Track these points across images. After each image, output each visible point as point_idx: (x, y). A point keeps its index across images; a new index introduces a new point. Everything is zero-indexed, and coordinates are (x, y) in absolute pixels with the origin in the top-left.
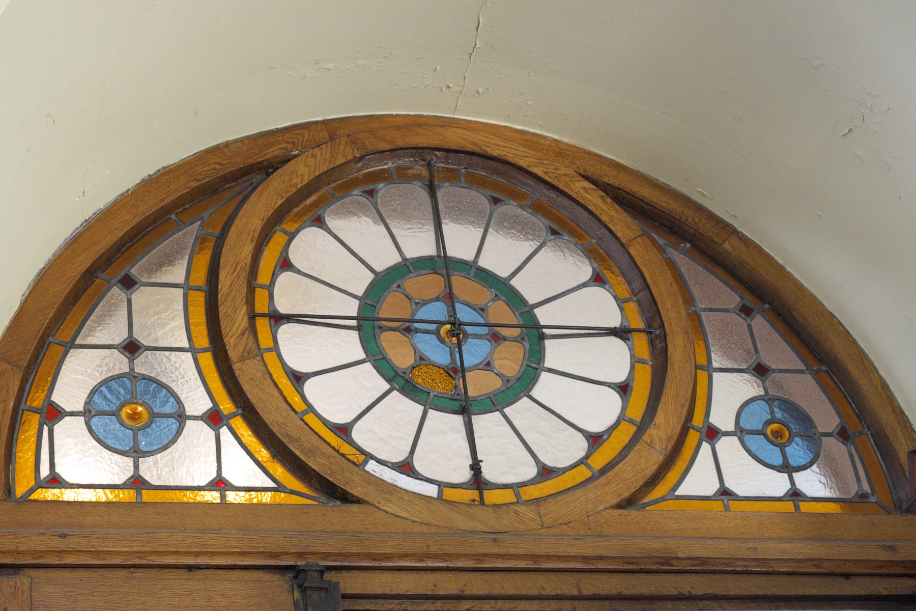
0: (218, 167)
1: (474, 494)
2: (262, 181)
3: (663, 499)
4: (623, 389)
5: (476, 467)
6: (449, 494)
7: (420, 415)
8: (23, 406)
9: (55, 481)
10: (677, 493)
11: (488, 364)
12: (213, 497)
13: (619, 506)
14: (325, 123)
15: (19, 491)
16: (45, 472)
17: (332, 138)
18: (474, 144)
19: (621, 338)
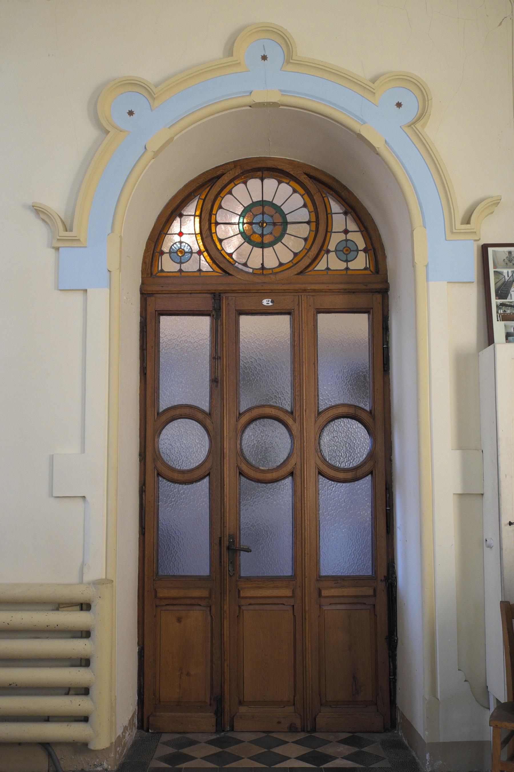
0: (204, 179)
1: (261, 271)
2: (217, 181)
3: (310, 271)
4: (306, 239)
5: (262, 264)
6: (255, 272)
7: (251, 248)
8: (155, 251)
9: (162, 271)
10: (315, 269)
11: (271, 233)
12: (198, 274)
13: (298, 274)
14: (234, 162)
15: (154, 273)
16: (160, 269)
17: (235, 167)
18: (274, 165)
19: (307, 224)
